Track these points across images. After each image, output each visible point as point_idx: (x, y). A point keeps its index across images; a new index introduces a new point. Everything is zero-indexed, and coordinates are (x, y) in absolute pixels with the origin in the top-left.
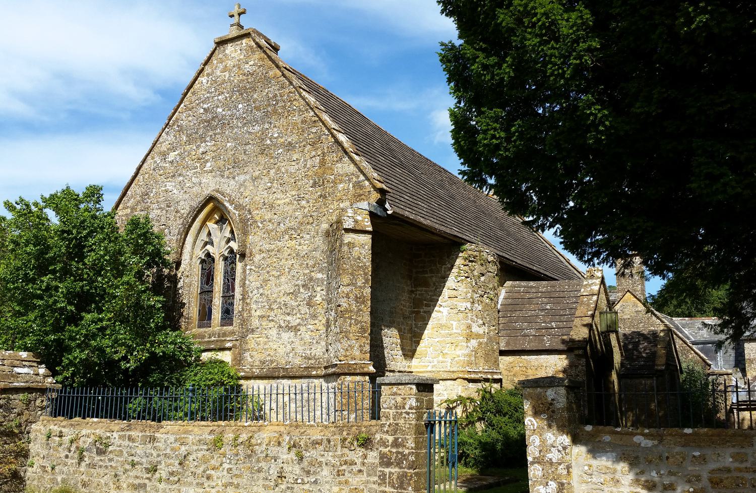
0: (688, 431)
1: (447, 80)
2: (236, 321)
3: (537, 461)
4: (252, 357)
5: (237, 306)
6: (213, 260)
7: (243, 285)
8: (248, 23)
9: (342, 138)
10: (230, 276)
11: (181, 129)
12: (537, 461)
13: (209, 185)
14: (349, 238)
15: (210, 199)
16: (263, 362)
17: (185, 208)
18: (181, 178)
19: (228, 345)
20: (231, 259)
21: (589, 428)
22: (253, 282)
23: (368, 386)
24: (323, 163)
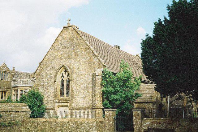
0: (162, 119)
1: (171, 3)
2: (70, 95)
3: (135, 125)
4: (74, 104)
5: (70, 92)
6: (64, 81)
7: (71, 87)
8: (71, 23)
9: (95, 52)
10: (68, 85)
11: (72, 114)
12: (135, 125)
13: (63, 62)
14: (97, 77)
15: (63, 66)
16: (77, 106)
17: (56, 68)
18: (55, 61)
19: (68, 101)
20: (69, 81)
21: (145, 119)
22: (74, 86)
23: (102, 111)
24: (91, 58)
